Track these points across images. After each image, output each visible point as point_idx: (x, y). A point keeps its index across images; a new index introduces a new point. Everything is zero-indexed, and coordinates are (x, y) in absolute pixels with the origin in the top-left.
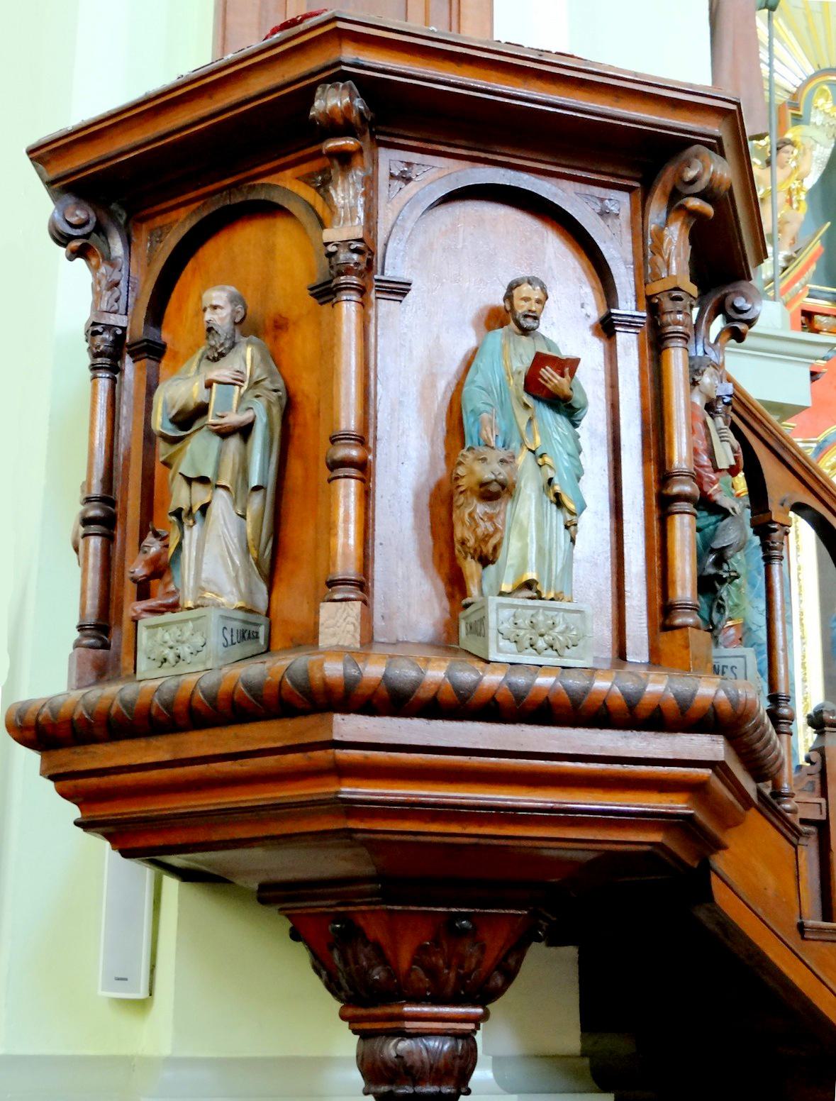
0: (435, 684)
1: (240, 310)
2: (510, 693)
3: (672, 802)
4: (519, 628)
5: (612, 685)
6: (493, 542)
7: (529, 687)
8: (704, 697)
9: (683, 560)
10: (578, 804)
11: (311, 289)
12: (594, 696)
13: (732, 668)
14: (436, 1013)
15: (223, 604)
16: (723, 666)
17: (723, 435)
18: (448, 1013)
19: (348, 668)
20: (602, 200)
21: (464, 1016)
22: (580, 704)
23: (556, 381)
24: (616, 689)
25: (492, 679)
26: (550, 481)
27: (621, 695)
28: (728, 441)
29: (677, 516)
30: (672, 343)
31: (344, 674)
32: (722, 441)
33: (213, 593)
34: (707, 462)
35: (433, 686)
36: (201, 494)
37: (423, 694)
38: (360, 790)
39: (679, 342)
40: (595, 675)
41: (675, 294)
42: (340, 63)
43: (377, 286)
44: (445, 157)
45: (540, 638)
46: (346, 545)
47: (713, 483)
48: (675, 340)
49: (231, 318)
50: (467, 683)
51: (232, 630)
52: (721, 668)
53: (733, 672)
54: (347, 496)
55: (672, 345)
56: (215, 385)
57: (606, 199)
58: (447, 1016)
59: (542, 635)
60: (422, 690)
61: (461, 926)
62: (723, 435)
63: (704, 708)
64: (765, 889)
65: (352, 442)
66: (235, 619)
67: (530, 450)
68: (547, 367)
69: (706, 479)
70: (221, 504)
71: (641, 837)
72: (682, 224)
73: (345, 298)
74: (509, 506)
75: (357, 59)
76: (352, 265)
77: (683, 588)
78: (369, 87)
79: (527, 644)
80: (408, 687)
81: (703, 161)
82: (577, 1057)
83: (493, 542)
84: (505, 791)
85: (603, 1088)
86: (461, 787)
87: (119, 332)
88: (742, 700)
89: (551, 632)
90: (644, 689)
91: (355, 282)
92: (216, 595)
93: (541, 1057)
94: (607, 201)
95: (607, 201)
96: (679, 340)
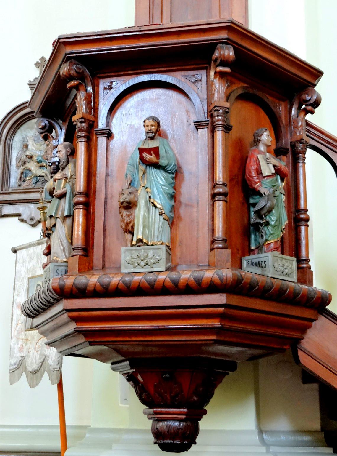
0: (93, 284)
1: (69, 150)
2: (125, 286)
3: (213, 322)
4: (132, 259)
5: (166, 277)
6: (131, 225)
7: (131, 282)
8: (207, 278)
9: (219, 220)
10: (184, 325)
11: (194, 122)
12: (158, 283)
13: (264, 261)
14: (167, 411)
15: (59, 261)
16: (261, 262)
17: (268, 161)
18: (172, 411)
19: (61, 282)
20: (194, 76)
21: (179, 413)
22: (130, 286)
23: (149, 158)
24: (168, 279)
25: (115, 280)
26: (150, 197)
27: (170, 281)
28: (270, 163)
29: (217, 202)
30: (217, 129)
31: (59, 284)
32: (268, 164)
33: (56, 257)
34: (255, 174)
35: (93, 285)
36: (53, 221)
37: (90, 288)
38: (84, 327)
39: (220, 128)
40: (92, 278)
41: (215, 109)
42: (66, 54)
43: (96, 133)
44: (133, 75)
45: (142, 261)
46: (78, 235)
47: (257, 183)
48: (217, 128)
49: (66, 153)
50: (106, 283)
51: (61, 270)
52: (260, 262)
53: (265, 264)
54: (79, 215)
55: (217, 130)
56: (57, 180)
57: (195, 75)
58: (172, 412)
59: (143, 260)
60: (89, 288)
61: (166, 376)
62: (268, 161)
63: (208, 283)
64: (334, 356)
65: (82, 195)
66: (62, 266)
67: (143, 187)
68: (144, 153)
69: (253, 182)
70: (59, 222)
71: (206, 338)
72: (219, 79)
73: (79, 141)
74: (133, 211)
75: (72, 51)
76: (80, 128)
77: (218, 232)
78: (82, 60)
79: (136, 265)
80: (83, 287)
81: (219, 51)
82: (319, 431)
83: (131, 225)
84: (140, 323)
85: (328, 444)
86: (122, 323)
87: (57, 164)
88: (225, 278)
89: (146, 259)
90: (180, 278)
91: (84, 134)
92: (57, 258)
93: (301, 431)
94: (196, 75)
95: (196, 75)
96: (220, 128)
